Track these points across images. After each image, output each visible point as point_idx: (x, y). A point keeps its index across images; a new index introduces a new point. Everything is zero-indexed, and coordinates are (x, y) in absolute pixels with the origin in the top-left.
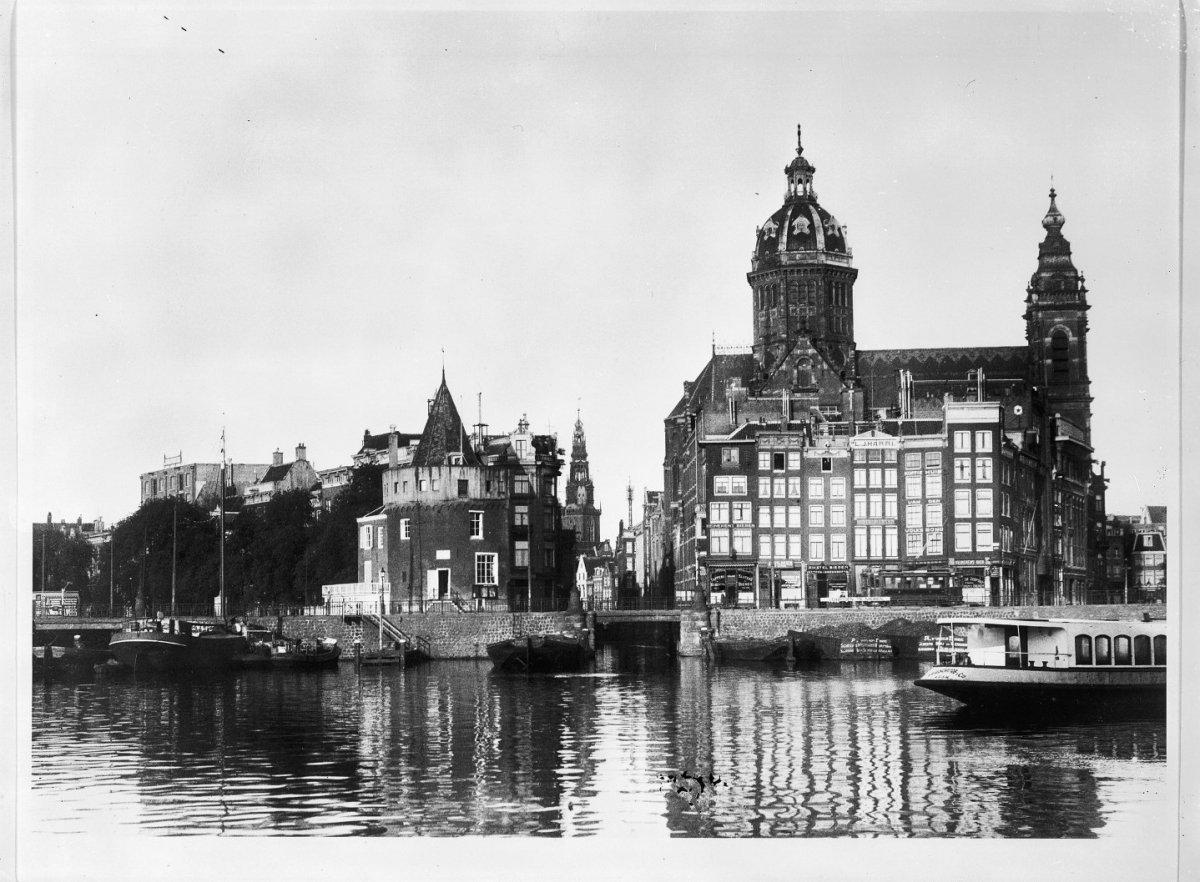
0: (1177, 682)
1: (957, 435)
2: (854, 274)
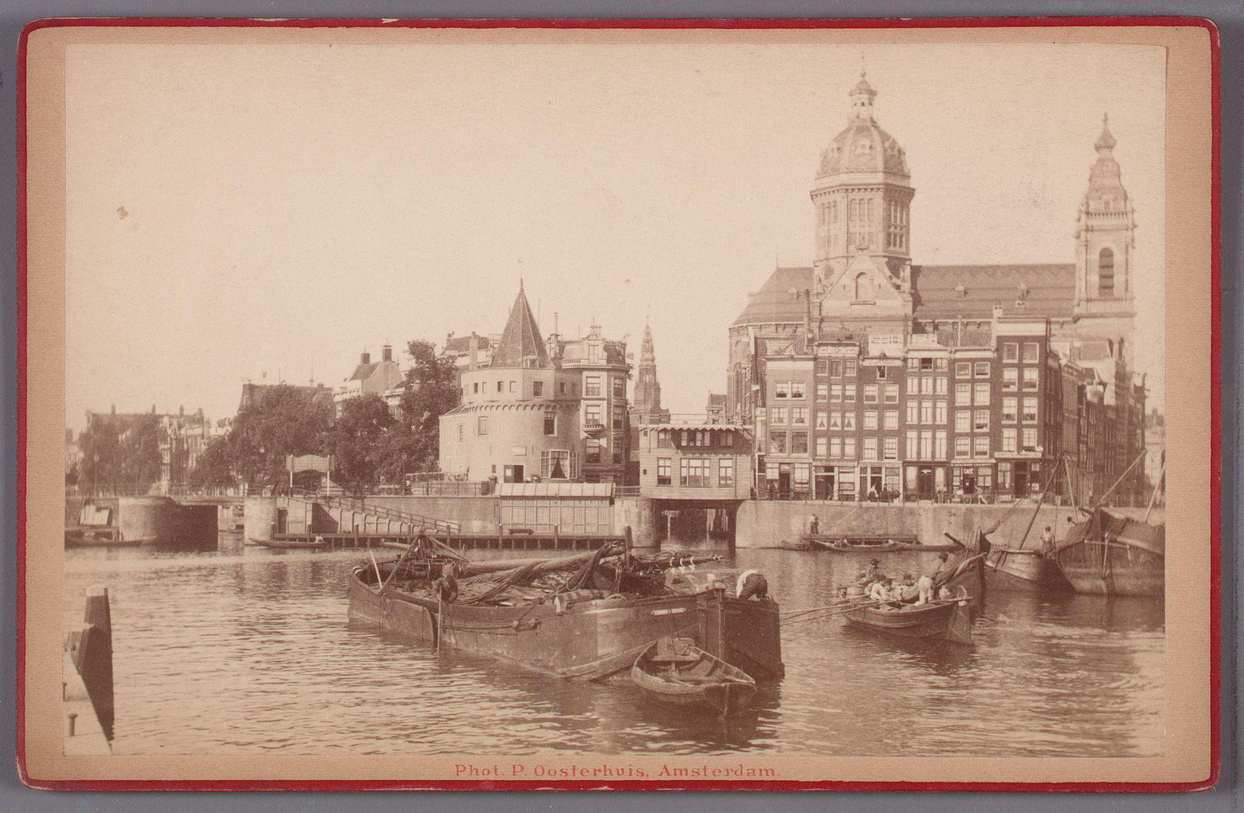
2: (911, 193)
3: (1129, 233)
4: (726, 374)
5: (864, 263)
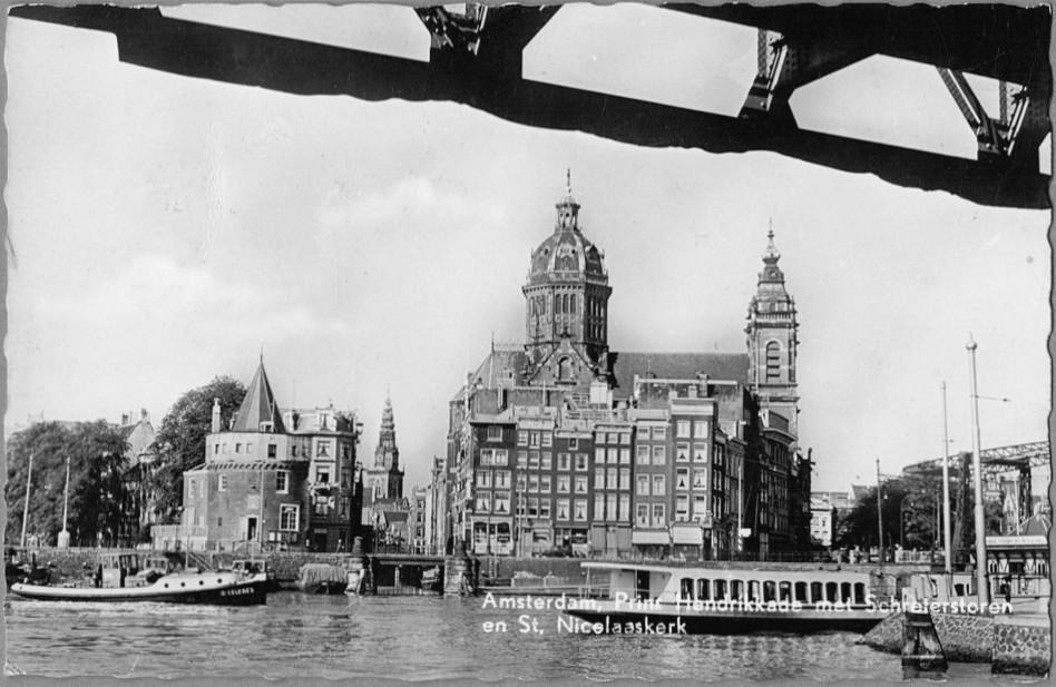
1: (680, 425)
2: (610, 290)
3: (792, 330)
4: (446, 441)
5: (566, 347)
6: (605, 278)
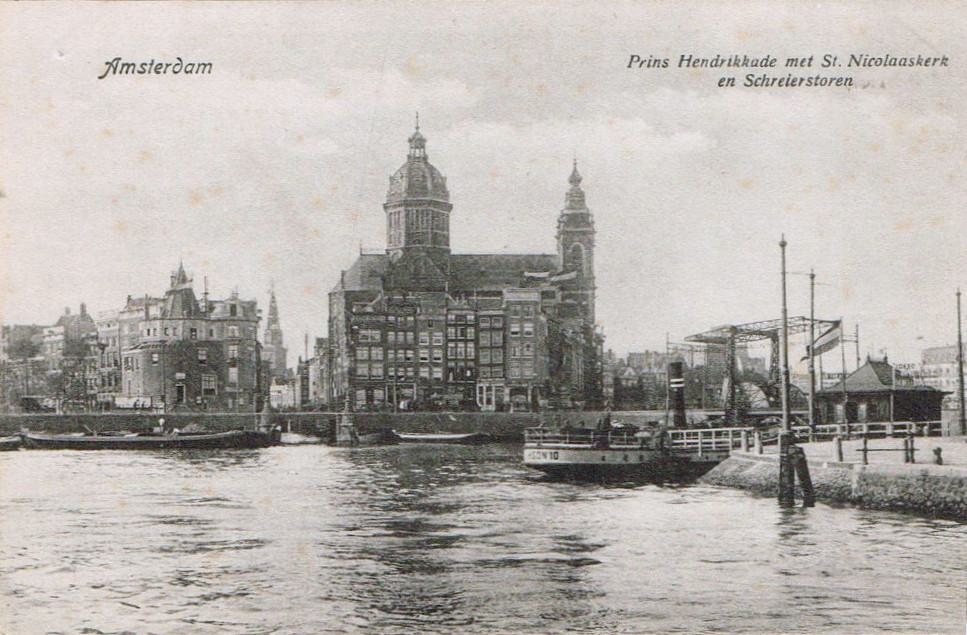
0: (962, 325)
6: (446, 195)
